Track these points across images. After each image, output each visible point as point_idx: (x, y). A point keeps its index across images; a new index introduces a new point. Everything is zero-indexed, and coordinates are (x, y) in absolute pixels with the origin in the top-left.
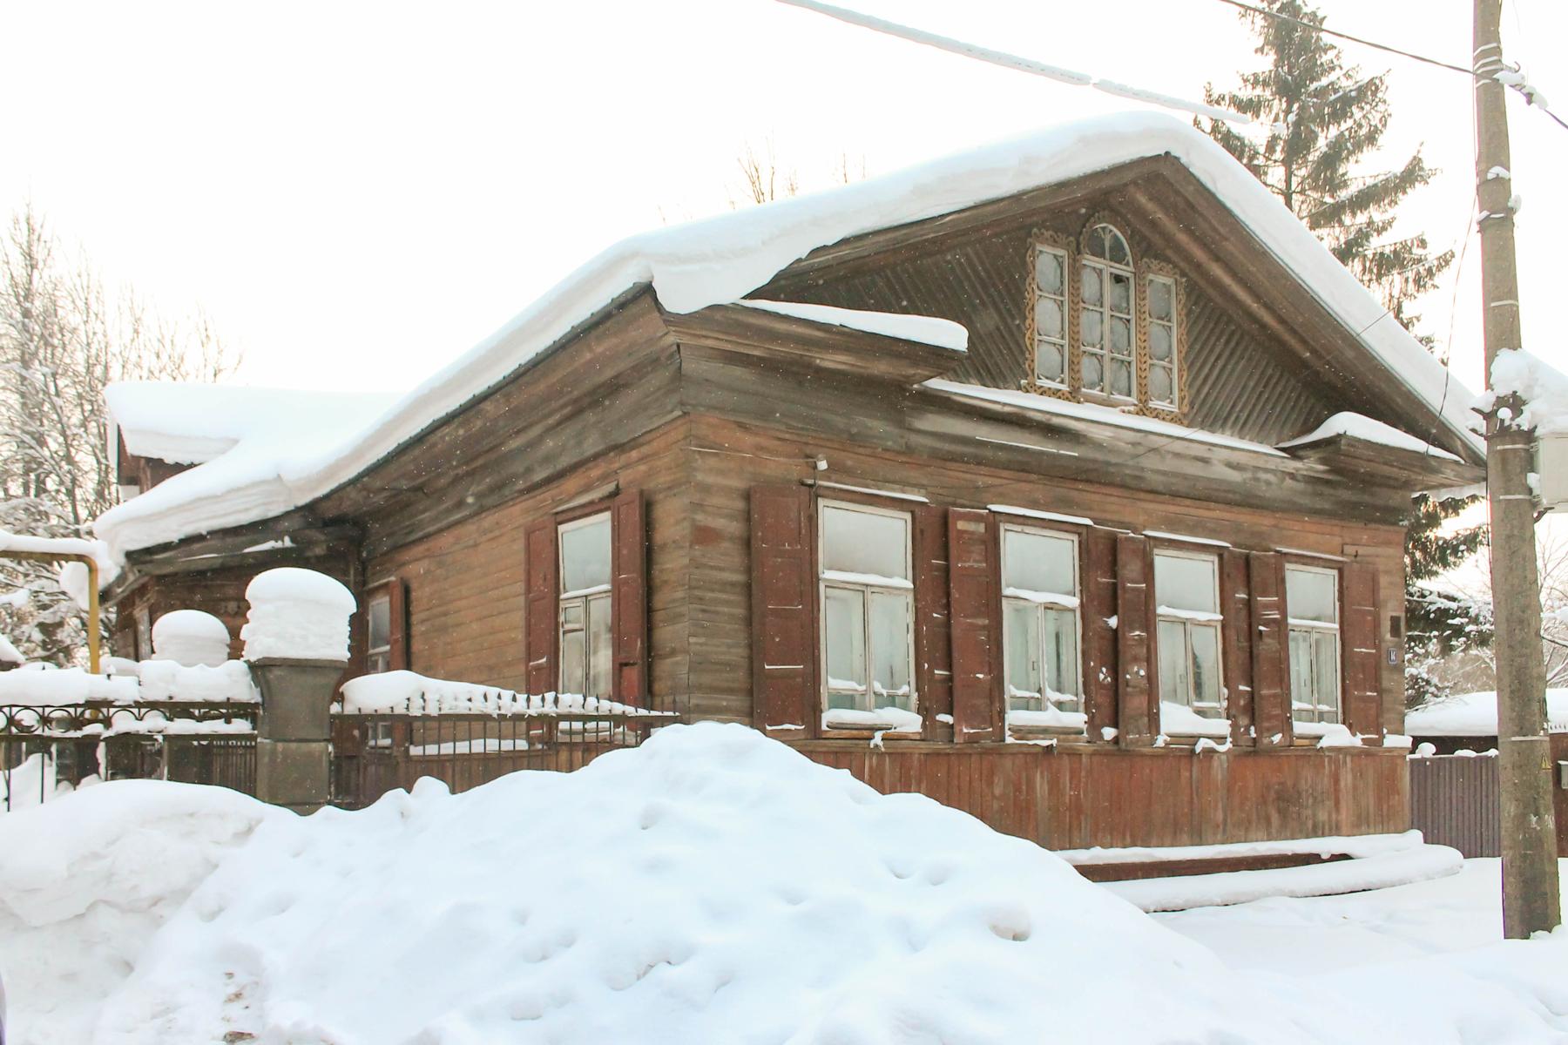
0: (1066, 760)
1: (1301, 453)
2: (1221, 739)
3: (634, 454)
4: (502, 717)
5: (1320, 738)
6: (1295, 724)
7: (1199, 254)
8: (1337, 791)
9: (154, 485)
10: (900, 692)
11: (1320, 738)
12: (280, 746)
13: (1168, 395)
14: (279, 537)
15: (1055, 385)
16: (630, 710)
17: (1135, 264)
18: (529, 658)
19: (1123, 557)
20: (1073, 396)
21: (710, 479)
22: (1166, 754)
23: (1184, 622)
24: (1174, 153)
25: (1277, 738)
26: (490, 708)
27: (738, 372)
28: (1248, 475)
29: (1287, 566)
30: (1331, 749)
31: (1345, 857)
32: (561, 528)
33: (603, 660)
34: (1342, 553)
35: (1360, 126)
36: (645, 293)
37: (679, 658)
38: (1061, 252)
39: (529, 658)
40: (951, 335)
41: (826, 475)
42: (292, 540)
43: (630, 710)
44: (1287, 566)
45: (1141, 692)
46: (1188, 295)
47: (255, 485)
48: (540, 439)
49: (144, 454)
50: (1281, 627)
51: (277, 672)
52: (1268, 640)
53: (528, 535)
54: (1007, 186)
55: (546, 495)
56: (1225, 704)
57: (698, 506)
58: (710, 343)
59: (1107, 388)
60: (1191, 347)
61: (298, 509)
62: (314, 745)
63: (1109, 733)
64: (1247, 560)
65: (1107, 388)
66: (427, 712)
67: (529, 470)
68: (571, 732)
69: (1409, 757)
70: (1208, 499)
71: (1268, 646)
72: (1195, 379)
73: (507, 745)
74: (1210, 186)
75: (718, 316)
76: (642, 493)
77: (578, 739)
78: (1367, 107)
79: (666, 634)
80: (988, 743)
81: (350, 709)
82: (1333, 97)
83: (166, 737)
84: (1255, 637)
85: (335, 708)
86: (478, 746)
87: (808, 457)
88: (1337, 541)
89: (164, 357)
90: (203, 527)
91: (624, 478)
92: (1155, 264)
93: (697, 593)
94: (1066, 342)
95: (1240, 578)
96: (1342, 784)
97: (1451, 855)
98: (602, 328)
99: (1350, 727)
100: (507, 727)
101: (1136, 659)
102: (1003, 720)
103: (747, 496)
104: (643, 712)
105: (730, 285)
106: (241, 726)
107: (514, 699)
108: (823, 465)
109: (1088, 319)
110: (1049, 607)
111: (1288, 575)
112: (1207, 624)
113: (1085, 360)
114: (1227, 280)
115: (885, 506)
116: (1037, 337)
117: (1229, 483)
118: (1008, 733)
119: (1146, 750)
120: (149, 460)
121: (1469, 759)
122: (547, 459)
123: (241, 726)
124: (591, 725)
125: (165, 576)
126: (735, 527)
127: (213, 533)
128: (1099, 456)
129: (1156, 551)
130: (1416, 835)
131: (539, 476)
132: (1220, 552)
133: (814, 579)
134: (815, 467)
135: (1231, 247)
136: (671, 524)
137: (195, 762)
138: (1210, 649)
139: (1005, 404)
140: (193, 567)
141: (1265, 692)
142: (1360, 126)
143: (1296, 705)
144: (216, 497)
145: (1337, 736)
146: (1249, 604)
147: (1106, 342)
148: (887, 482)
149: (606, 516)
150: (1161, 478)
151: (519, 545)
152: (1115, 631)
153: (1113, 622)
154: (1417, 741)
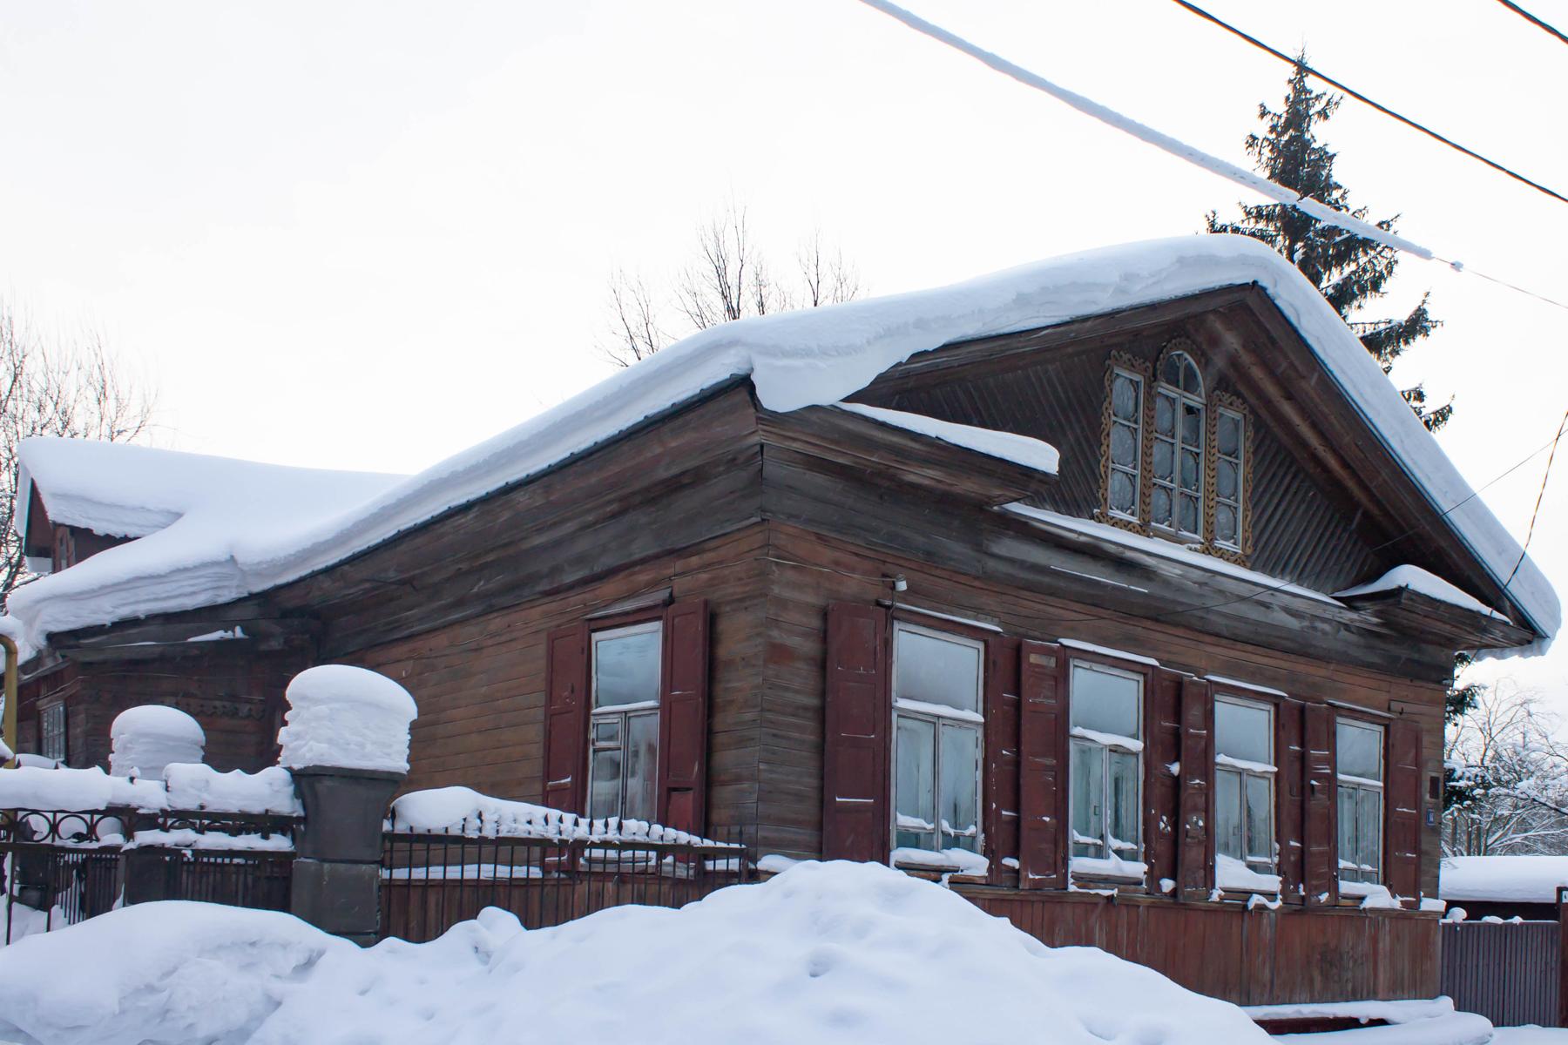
0: (1124, 911)
1: (1359, 604)
2: (1271, 896)
3: (694, 560)
4: (563, 842)
5: (1362, 898)
6: (1341, 883)
7: (1271, 390)
8: (1375, 953)
9: (80, 559)
10: (967, 833)
11: (1362, 898)
12: (326, 866)
13: (1232, 537)
14: (229, 627)
15: (1126, 517)
16: (684, 837)
17: (1208, 396)
18: (548, 776)
19: (1186, 701)
20: (1143, 530)
21: (787, 594)
22: (1220, 909)
23: (1240, 773)
24: (1263, 282)
25: (1324, 897)
26: (551, 833)
27: (820, 479)
28: (1306, 623)
29: (1217, 697)
30: (1373, 910)
31: (1382, 1022)
32: (596, 636)
33: (1345, 809)
34: (1389, 710)
35: (1365, 270)
36: (743, 385)
37: (745, 785)
38: (1137, 377)
39: (548, 776)
40: (1041, 456)
41: (904, 597)
42: (243, 631)
43: (684, 837)
44: (1339, 720)
45: (1200, 843)
46: (1256, 432)
47: (204, 565)
48: (572, 537)
49: (69, 522)
50: (1331, 781)
51: (328, 783)
52: (1319, 796)
53: (552, 640)
54: (1105, 302)
55: (575, 599)
56: (1276, 859)
57: (775, 622)
58: (796, 446)
59: (1176, 523)
60: (1256, 487)
61: (252, 596)
62: (364, 867)
63: (1167, 885)
64: (1302, 710)
65: (1176, 523)
66: (484, 833)
67: (556, 570)
68: (604, 861)
69: (1442, 921)
70: (1269, 646)
71: (1317, 803)
72: (1260, 517)
73: (520, 872)
74: (1293, 320)
75: (814, 417)
76: (706, 603)
77: (611, 869)
78: (1372, 253)
79: (726, 759)
80: (1050, 891)
81: (401, 828)
82: (1338, 239)
83: (196, 853)
84: (1307, 790)
85: (387, 826)
86: (471, 872)
87: (884, 575)
88: (1383, 697)
89: (50, 408)
90: (142, 610)
91: (681, 585)
92: (1226, 397)
93: (769, 716)
94: (1138, 472)
95: (1294, 733)
96: (1381, 945)
97: (1478, 1023)
98: (679, 422)
99: (1390, 888)
100: (505, 851)
101: (1195, 810)
102: (1066, 865)
103: (824, 614)
104: (695, 840)
105: (828, 383)
106: (279, 843)
107: (576, 824)
108: (902, 586)
109: (1159, 452)
110: (1115, 749)
111: (1339, 728)
112: (1262, 776)
113: (1155, 492)
114: (1296, 419)
115: (960, 634)
116: (1111, 465)
117: (1290, 630)
118: (1071, 881)
119: (1201, 904)
120: (74, 530)
121: (1495, 925)
122: (580, 560)
123: (279, 843)
124: (627, 854)
125: (91, 663)
126: (809, 647)
127: (153, 618)
128: (1168, 595)
129: (1217, 697)
130: (1446, 1002)
131: (569, 578)
132: (1276, 701)
133: (888, 707)
134: (893, 587)
135: (1310, 385)
136: (739, 636)
137: (262, 884)
138: (1264, 802)
139: (1081, 534)
140: (126, 656)
141: (1314, 849)
142: (1365, 270)
143: (1342, 864)
144: (160, 576)
145: (1379, 897)
146: (1303, 757)
147: (1177, 475)
148: (962, 608)
149: (657, 626)
150: (1294, 623)
151: (541, 650)
152: (1176, 781)
153: (1175, 768)
154: (1451, 904)
